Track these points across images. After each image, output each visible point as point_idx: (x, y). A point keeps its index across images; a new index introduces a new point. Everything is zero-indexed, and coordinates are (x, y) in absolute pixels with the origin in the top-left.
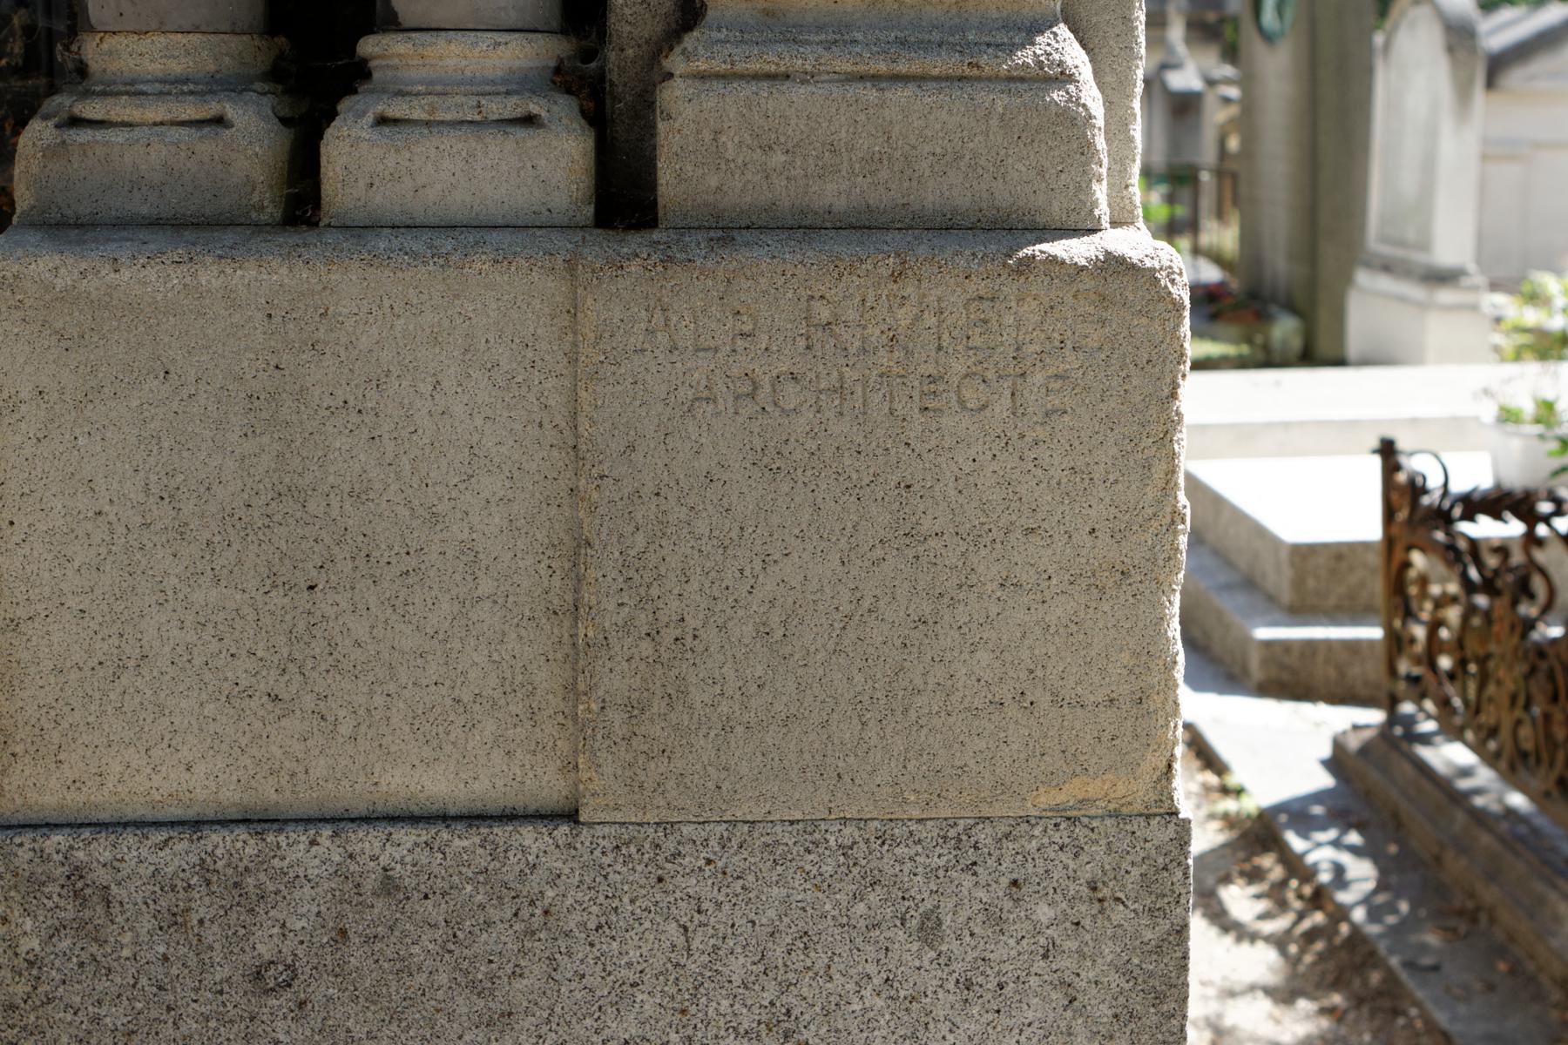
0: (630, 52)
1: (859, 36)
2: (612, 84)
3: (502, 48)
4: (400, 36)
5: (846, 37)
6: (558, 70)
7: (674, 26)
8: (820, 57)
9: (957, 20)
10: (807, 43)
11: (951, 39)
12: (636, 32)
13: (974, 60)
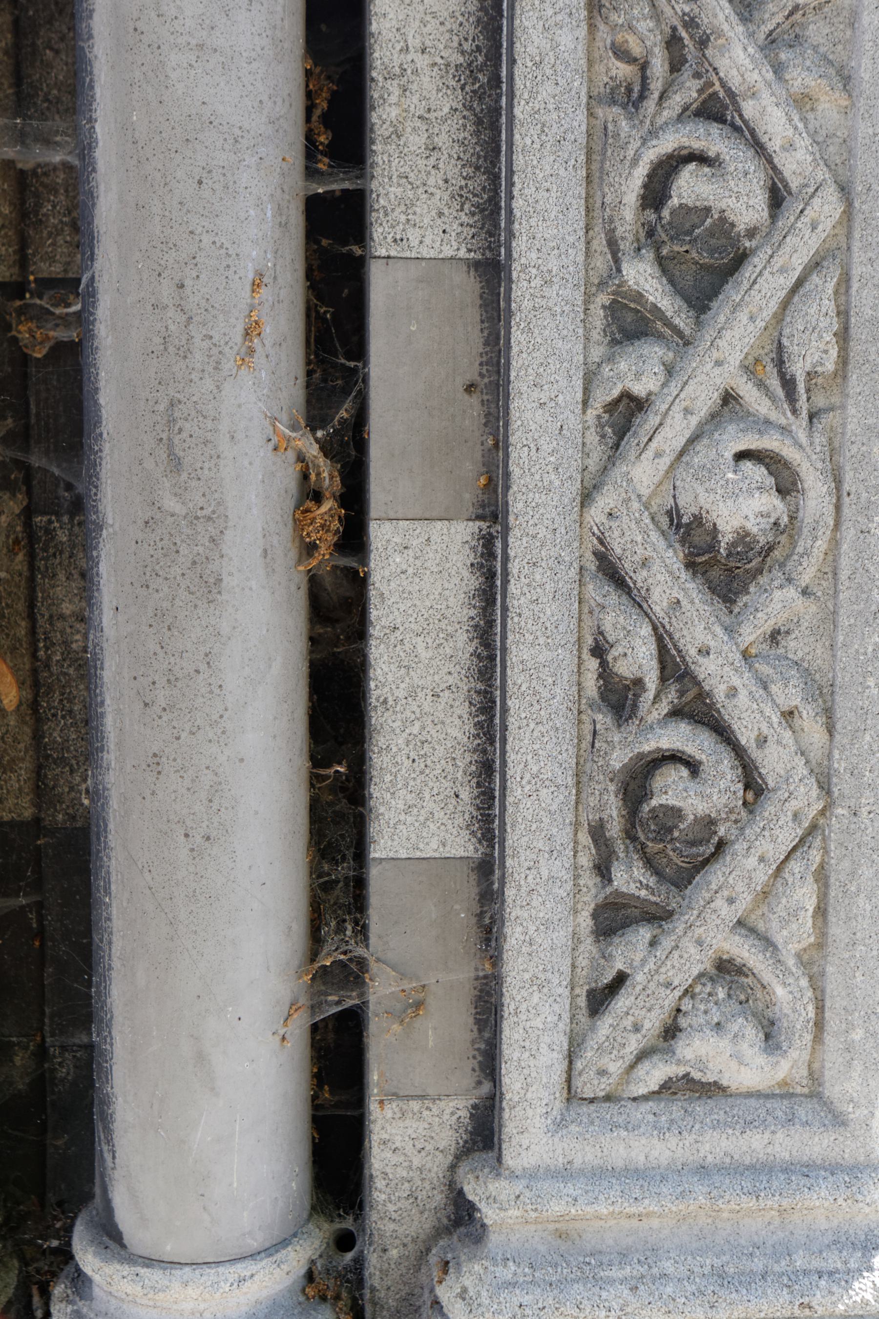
0: (394, 1253)
1: (668, 1266)
2: (373, 1289)
3: (248, 1284)
4: (126, 1269)
5: (655, 1270)
6: (310, 1276)
7: (445, 1221)
8: (626, 1304)
9: (781, 1235)
10: (611, 1281)
11: (777, 1268)
12: (401, 1230)
13: (806, 1300)
